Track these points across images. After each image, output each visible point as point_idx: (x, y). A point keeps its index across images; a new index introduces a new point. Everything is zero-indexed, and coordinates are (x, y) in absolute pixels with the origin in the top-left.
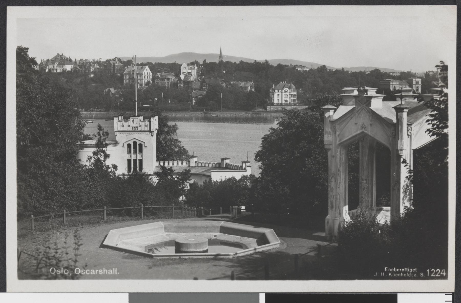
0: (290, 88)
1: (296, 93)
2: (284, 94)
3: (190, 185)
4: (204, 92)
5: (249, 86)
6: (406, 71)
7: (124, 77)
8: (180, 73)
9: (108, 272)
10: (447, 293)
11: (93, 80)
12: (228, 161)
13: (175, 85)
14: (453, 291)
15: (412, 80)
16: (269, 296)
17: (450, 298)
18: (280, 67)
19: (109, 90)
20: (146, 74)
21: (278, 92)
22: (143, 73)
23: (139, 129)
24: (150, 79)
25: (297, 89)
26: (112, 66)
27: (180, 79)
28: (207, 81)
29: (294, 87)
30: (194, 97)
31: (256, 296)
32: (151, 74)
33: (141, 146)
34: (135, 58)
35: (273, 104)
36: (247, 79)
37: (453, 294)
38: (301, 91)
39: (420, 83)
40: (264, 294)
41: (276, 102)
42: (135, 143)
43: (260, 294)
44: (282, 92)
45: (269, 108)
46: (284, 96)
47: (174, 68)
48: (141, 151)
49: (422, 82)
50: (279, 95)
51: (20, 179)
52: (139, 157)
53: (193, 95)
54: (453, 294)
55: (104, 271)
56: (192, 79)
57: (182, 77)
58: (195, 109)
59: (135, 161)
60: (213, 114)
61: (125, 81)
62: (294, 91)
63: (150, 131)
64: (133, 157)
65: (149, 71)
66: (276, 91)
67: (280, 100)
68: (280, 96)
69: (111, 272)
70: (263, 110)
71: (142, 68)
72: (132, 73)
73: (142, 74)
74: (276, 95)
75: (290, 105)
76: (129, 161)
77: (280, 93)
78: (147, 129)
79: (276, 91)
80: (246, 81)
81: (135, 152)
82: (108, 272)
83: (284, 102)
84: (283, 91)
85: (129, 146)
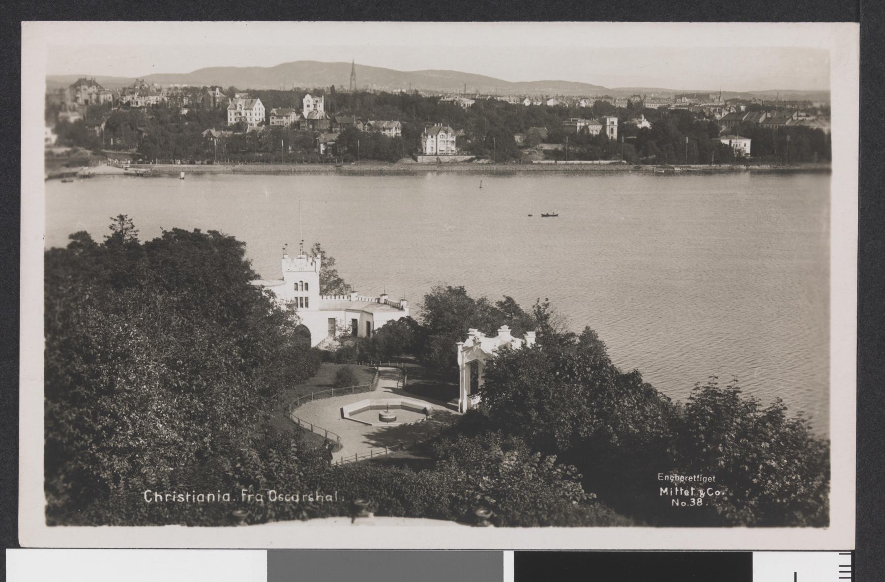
0: (446, 132)
2: (439, 139)
4: (335, 137)
5: (393, 130)
8: (302, 106)
10: (842, 552)
11: (187, 117)
13: (296, 125)
14: (854, 548)
16: (522, 557)
17: (847, 560)
18: (434, 100)
19: (210, 134)
24: (263, 116)
25: (456, 129)
26: (212, 100)
27: (302, 117)
28: (338, 119)
31: (497, 555)
33: (307, 284)
34: (642, 95)
35: (425, 155)
36: (391, 118)
37: (853, 553)
38: (461, 132)
39: (616, 123)
40: (512, 552)
41: (428, 151)
43: (505, 552)
45: (420, 159)
48: (307, 289)
51: (52, 391)
53: (321, 140)
54: (853, 553)
56: (317, 117)
57: (306, 113)
58: (324, 160)
59: (301, 298)
60: (346, 167)
62: (452, 135)
65: (262, 106)
70: (414, 162)
75: (447, 154)
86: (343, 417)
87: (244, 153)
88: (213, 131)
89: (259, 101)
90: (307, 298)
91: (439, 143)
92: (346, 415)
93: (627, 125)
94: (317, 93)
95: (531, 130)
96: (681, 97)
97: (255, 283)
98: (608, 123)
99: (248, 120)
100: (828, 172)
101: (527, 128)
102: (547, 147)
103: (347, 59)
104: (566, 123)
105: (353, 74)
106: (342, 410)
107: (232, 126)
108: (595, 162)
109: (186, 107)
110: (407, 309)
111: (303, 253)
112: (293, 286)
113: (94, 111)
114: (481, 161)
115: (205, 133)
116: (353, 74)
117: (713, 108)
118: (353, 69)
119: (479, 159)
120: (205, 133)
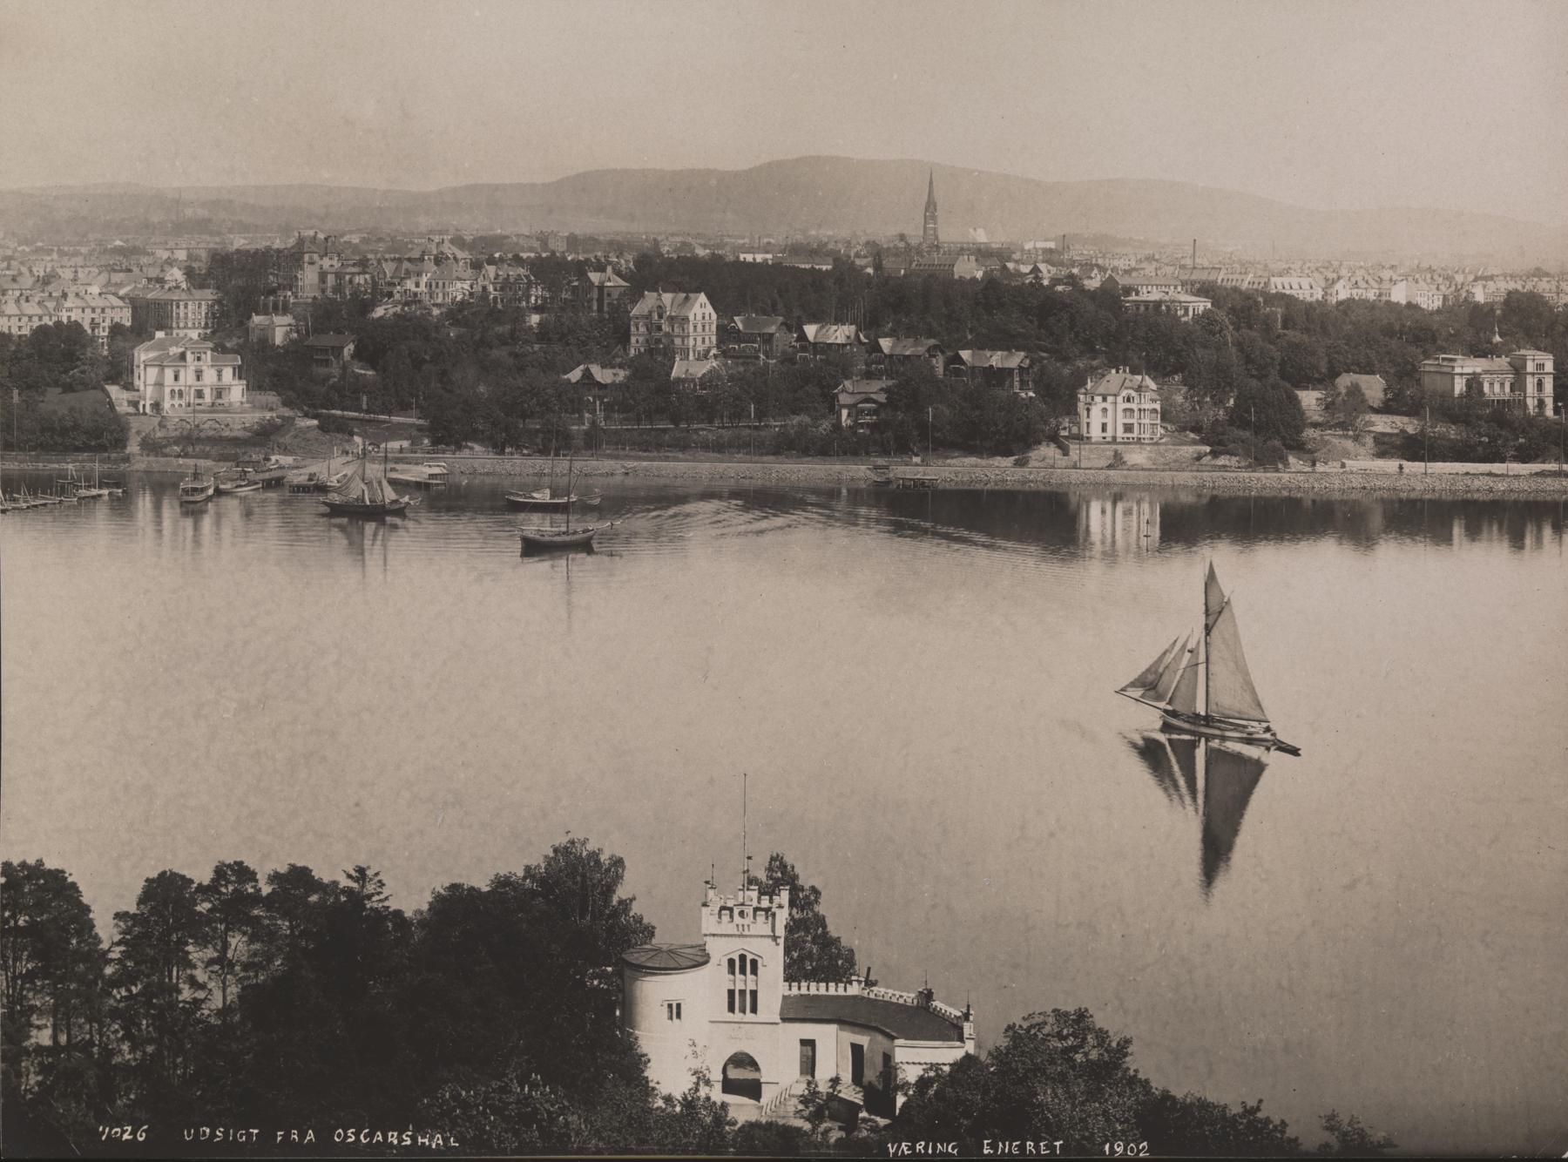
1: (1157, 406)
3: (832, 407)
7: (633, 329)
11: (543, 334)
20: (699, 317)
21: (1104, 400)
22: (691, 318)
25: (423, 923)
29: (1153, 386)
30: (845, 406)
32: (714, 317)
33: (754, 963)
36: (1007, 342)
41: (1096, 433)
42: (743, 958)
48: (754, 971)
49: (1556, 366)
52: (751, 986)
59: (742, 992)
62: (1154, 401)
64: (739, 986)
65: (709, 309)
66: (1098, 399)
67: (1110, 428)
68: (1110, 413)
71: (687, 298)
73: (686, 319)
74: (1096, 411)
76: (731, 993)
79: (1098, 399)
80: (1008, 349)
81: (743, 971)
83: (1120, 433)
84: (1120, 399)
85: (731, 962)
89: (702, 298)
90: (754, 994)
91: (1119, 412)
95: (1344, 381)
98: (1530, 367)
99: (678, 341)
101: (1334, 374)
102: (1383, 424)
104: (1428, 365)
108: (1497, 468)
109: (538, 309)
111: (750, 882)
113: (341, 313)
114: (1222, 460)
115: (575, 375)
117: (1144, 541)
119: (1215, 454)
120: (575, 375)
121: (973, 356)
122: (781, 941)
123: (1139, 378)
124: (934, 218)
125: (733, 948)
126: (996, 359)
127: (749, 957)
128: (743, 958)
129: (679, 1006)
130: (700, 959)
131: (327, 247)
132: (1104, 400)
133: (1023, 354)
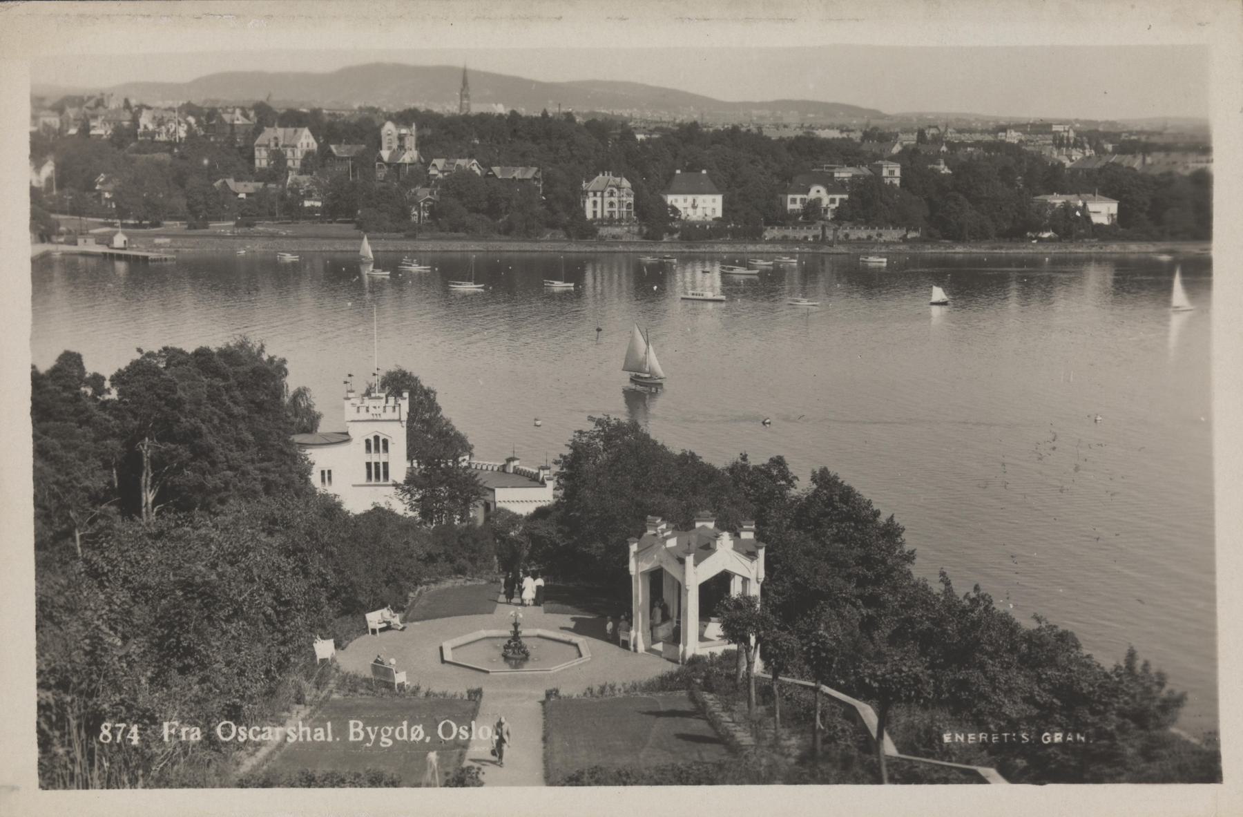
2: (607, 200)
6: (652, 437)
9: (313, 733)
12: (516, 463)
15: (881, 167)
21: (595, 195)
23: (384, 417)
33: (385, 442)
36: (522, 160)
42: (376, 438)
44: (602, 197)
46: (606, 205)
47: (363, 130)
48: (386, 448)
49: (902, 171)
50: (595, 203)
55: (301, 729)
59: (377, 464)
61: (257, 162)
63: (399, 420)
69: (322, 734)
72: (272, 144)
76: (368, 465)
77: (599, 200)
78: (397, 417)
81: (378, 477)
82: (313, 733)
85: (368, 441)
86: (443, 661)
87: (670, 690)
88: (231, 182)
90: (386, 465)
92: (448, 656)
93: (932, 169)
94: (404, 118)
96: (1004, 129)
97: (464, 461)
100: (1199, 272)
103: (459, 63)
105: (465, 83)
106: (441, 649)
107: (261, 170)
110: (384, 430)
112: (364, 445)
116: (465, 83)
118: (465, 79)
120: (217, 184)
121: (502, 172)
122: (405, 424)
123: (618, 179)
124: (467, 96)
125: (369, 431)
126: (518, 173)
127: (381, 438)
128: (376, 438)
129: (329, 472)
130: (343, 438)
131: (38, 723)
132: (595, 195)
133: (535, 169)
